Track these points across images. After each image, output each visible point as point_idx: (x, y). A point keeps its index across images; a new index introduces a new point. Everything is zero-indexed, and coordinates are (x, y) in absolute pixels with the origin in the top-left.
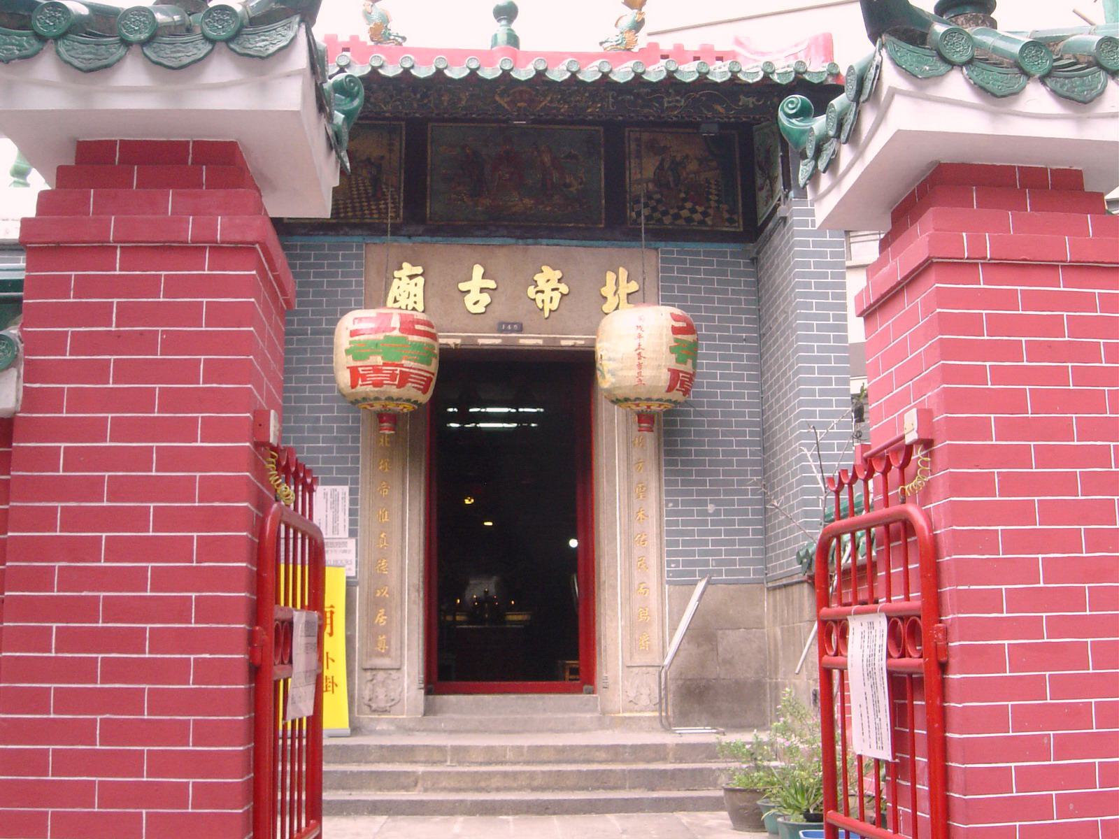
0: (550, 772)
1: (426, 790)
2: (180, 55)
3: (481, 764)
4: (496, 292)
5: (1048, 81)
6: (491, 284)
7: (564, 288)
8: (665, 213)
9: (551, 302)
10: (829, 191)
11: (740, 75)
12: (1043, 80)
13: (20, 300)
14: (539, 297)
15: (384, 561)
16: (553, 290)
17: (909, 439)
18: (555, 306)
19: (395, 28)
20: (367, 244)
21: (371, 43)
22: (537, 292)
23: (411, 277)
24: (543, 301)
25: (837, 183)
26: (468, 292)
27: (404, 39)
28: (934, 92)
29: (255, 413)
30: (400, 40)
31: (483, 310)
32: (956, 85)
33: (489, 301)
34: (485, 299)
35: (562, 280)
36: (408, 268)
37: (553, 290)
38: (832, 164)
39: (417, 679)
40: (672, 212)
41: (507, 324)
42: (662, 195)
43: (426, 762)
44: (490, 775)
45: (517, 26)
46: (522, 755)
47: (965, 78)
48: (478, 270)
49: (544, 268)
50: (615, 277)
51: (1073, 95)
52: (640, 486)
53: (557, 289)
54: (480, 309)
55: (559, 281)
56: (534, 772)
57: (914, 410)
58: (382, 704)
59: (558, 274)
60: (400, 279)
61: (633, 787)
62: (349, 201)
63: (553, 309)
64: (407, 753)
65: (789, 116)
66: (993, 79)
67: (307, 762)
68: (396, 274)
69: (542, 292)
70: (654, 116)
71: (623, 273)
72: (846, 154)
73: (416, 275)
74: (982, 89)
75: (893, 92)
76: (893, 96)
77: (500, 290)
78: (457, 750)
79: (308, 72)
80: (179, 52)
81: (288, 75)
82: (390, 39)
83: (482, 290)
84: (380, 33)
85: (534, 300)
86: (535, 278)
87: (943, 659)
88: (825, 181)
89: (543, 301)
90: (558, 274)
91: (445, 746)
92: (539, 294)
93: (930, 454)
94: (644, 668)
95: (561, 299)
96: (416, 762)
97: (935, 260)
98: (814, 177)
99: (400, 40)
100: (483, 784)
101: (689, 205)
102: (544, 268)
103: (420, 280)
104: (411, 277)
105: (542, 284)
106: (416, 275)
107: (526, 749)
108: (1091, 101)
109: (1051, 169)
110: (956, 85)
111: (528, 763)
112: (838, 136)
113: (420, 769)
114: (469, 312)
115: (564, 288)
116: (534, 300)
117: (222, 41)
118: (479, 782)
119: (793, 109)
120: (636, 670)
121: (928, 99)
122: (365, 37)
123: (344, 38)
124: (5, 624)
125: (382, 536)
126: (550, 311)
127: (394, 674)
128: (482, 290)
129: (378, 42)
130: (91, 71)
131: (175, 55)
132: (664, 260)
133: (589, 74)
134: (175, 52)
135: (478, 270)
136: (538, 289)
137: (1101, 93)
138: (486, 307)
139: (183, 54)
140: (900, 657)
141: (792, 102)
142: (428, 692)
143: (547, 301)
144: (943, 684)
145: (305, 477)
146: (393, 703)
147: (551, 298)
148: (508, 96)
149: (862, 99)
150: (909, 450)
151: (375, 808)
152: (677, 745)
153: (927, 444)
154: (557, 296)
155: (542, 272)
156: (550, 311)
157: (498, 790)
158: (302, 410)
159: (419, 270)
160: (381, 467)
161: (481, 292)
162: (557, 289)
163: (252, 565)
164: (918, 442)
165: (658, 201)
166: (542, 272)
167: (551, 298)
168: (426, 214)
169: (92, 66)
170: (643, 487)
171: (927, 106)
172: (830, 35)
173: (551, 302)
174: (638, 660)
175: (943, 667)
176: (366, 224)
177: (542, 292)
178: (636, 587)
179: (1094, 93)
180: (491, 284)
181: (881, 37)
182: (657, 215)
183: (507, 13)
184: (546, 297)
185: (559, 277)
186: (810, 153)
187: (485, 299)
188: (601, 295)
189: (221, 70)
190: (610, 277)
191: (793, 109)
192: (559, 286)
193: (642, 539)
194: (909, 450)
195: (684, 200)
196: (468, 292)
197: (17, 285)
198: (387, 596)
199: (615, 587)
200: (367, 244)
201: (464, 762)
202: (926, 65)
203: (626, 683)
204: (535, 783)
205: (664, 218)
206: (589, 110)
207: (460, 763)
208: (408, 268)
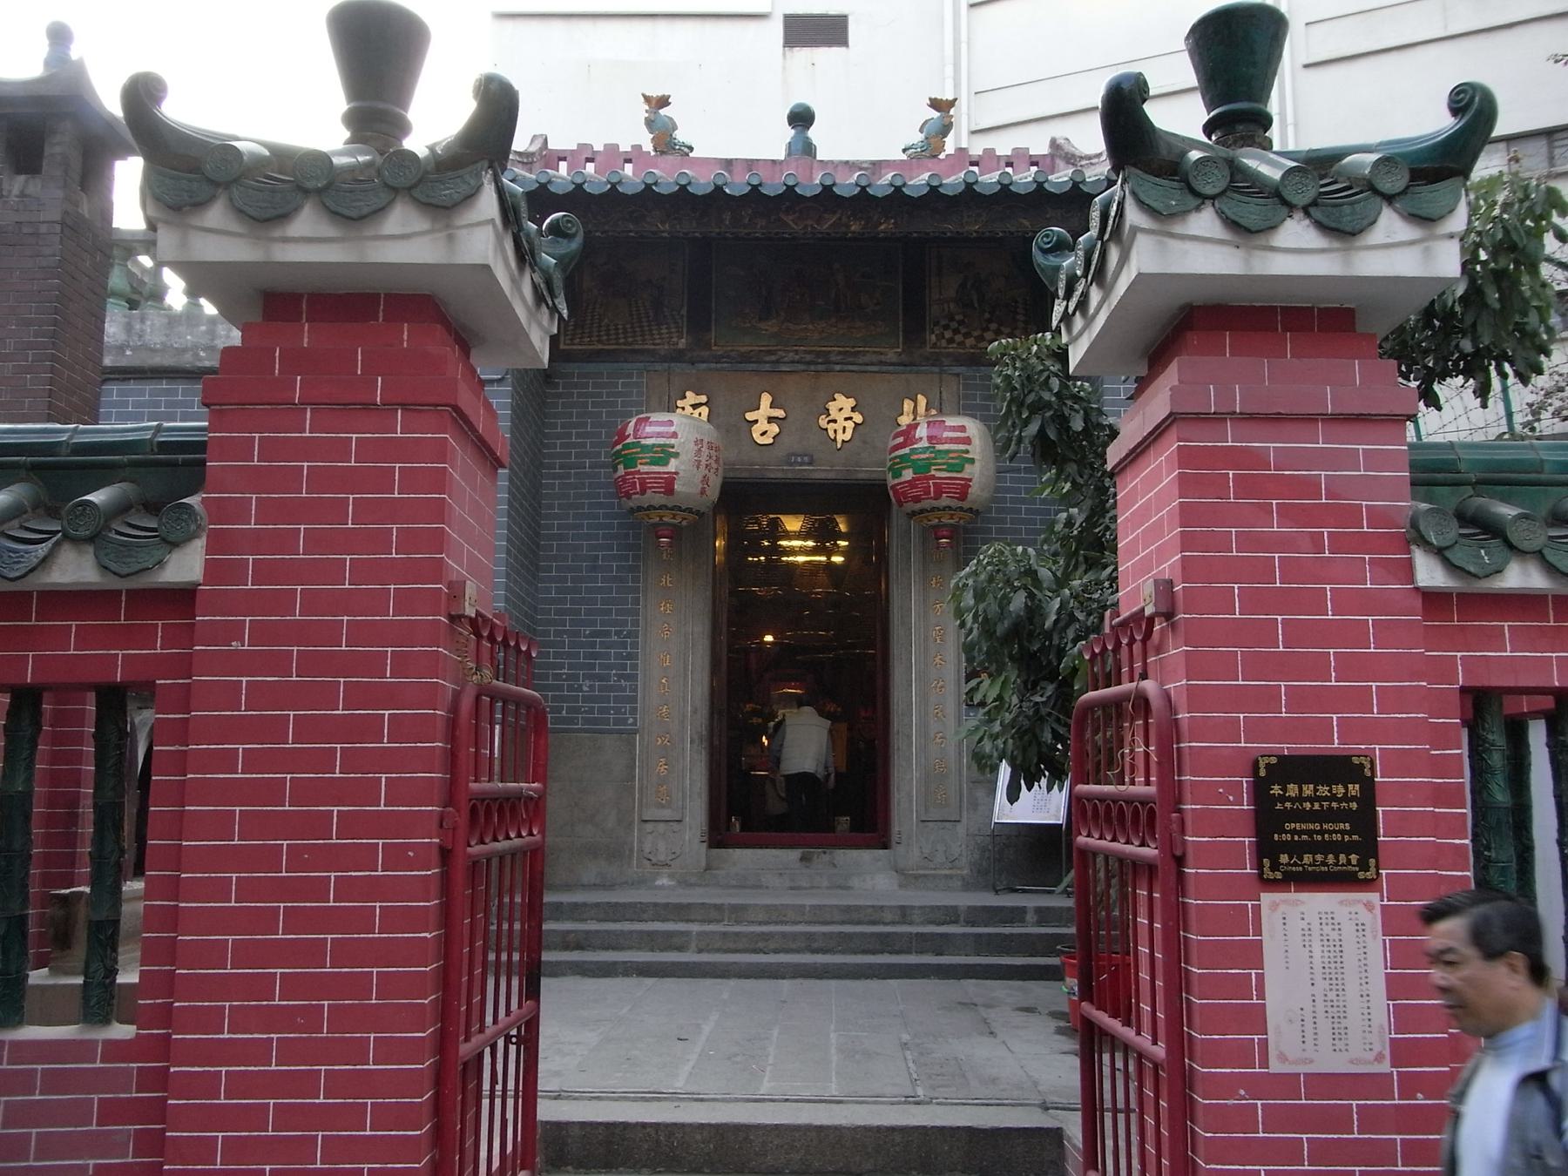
0: (832, 933)
1: (700, 951)
2: (358, 204)
3: (760, 923)
5: (1312, 210)
6: (780, 413)
7: (858, 418)
8: (967, 335)
9: (844, 432)
10: (1081, 333)
11: (1046, 185)
12: (1306, 210)
13: (203, 463)
14: (831, 427)
16: (846, 419)
17: (1149, 611)
18: (847, 436)
19: (681, 136)
20: (648, 371)
21: (653, 153)
22: (829, 422)
23: (695, 406)
24: (835, 431)
25: (1089, 321)
26: (756, 421)
27: (691, 149)
28: (1178, 229)
29: (450, 585)
30: (686, 150)
31: (771, 441)
32: (1204, 222)
33: (777, 430)
34: (775, 429)
36: (691, 397)
37: (846, 419)
38: (1083, 305)
40: (975, 334)
41: (796, 455)
42: (965, 316)
43: (703, 921)
44: (770, 936)
45: (813, 133)
46: (804, 914)
47: (1217, 212)
48: (766, 400)
49: (836, 396)
50: (912, 404)
51: (1341, 227)
53: (850, 418)
54: (768, 440)
55: (853, 409)
56: (815, 933)
57: (1152, 580)
58: (662, 858)
59: (852, 402)
60: (683, 408)
61: (921, 952)
62: (628, 326)
64: (681, 911)
65: (1045, 252)
66: (1250, 212)
68: (680, 403)
70: (951, 232)
71: (922, 400)
72: (1095, 295)
73: (701, 405)
74: (1232, 224)
75: (1135, 230)
76: (1135, 235)
77: (789, 420)
78: (736, 909)
79: (498, 221)
80: (360, 200)
81: (479, 224)
82: (674, 149)
83: (771, 420)
84: (666, 141)
85: (826, 429)
87: (1178, 853)
88: (1078, 322)
89: (835, 431)
90: (852, 402)
91: (723, 905)
93: (1173, 626)
96: (692, 921)
97: (1178, 416)
98: (1067, 318)
99: (686, 150)
100: (761, 945)
101: (993, 326)
102: (836, 396)
103: (705, 410)
104: (695, 406)
105: (834, 414)
106: (701, 405)
107: (808, 909)
108: (1361, 231)
109: (1318, 308)
110: (1204, 222)
111: (809, 923)
112: (1086, 277)
113: (695, 928)
115: (858, 418)
116: (826, 429)
117: (404, 188)
118: (757, 943)
119: (1049, 243)
120: (930, 824)
121: (1172, 236)
122: (648, 147)
123: (625, 147)
124: (187, 808)
126: (843, 441)
127: (675, 826)
128: (771, 420)
129: (663, 153)
130: (267, 220)
131: (354, 204)
132: (966, 387)
133: (883, 183)
134: (354, 201)
135: (766, 400)
136: (830, 418)
137: (1374, 222)
139: (362, 203)
140: (1140, 846)
141: (1047, 236)
142: (711, 846)
143: (840, 431)
144: (1181, 877)
145: (517, 644)
146: (674, 856)
147: (844, 428)
148: (794, 213)
149: (1106, 237)
150: (1151, 621)
151: (645, 971)
152: (969, 907)
153: (1169, 616)
154: (850, 425)
155: (835, 400)
157: (776, 951)
159: (703, 399)
161: (769, 422)
162: (850, 418)
163: (447, 744)
164: (1157, 614)
165: (961, 323)
166: (835, 400)
167: (844, 428)
169: (268, 216)
170: (939, 630)
171: (1174, 244)
173: (844, 432)
174: (935, 814)
175: (1180, 861)
176: (648, 351)
177: (835, 421)
178: (932, 736)
179: (1365, 222)
180: (780, 413)
181: (1124, 169)
182: (959, 338)
183: (801, 118)
186: (1061, 293)
187: (775, 429)
189: (401, 218)
190: (908, 405)
191: (1049, 243)
192: (853, 415)
194: (1151, 621)
195: (990, 321)
196: (756, 421)
197: (201, 447)
200: (648, 371)
201: (741, 922)
202: (1172, 199)
204: (815, 945)
205: (985, 334)
206: (882, 227)
207: (738, 922)
208: (691, 397)
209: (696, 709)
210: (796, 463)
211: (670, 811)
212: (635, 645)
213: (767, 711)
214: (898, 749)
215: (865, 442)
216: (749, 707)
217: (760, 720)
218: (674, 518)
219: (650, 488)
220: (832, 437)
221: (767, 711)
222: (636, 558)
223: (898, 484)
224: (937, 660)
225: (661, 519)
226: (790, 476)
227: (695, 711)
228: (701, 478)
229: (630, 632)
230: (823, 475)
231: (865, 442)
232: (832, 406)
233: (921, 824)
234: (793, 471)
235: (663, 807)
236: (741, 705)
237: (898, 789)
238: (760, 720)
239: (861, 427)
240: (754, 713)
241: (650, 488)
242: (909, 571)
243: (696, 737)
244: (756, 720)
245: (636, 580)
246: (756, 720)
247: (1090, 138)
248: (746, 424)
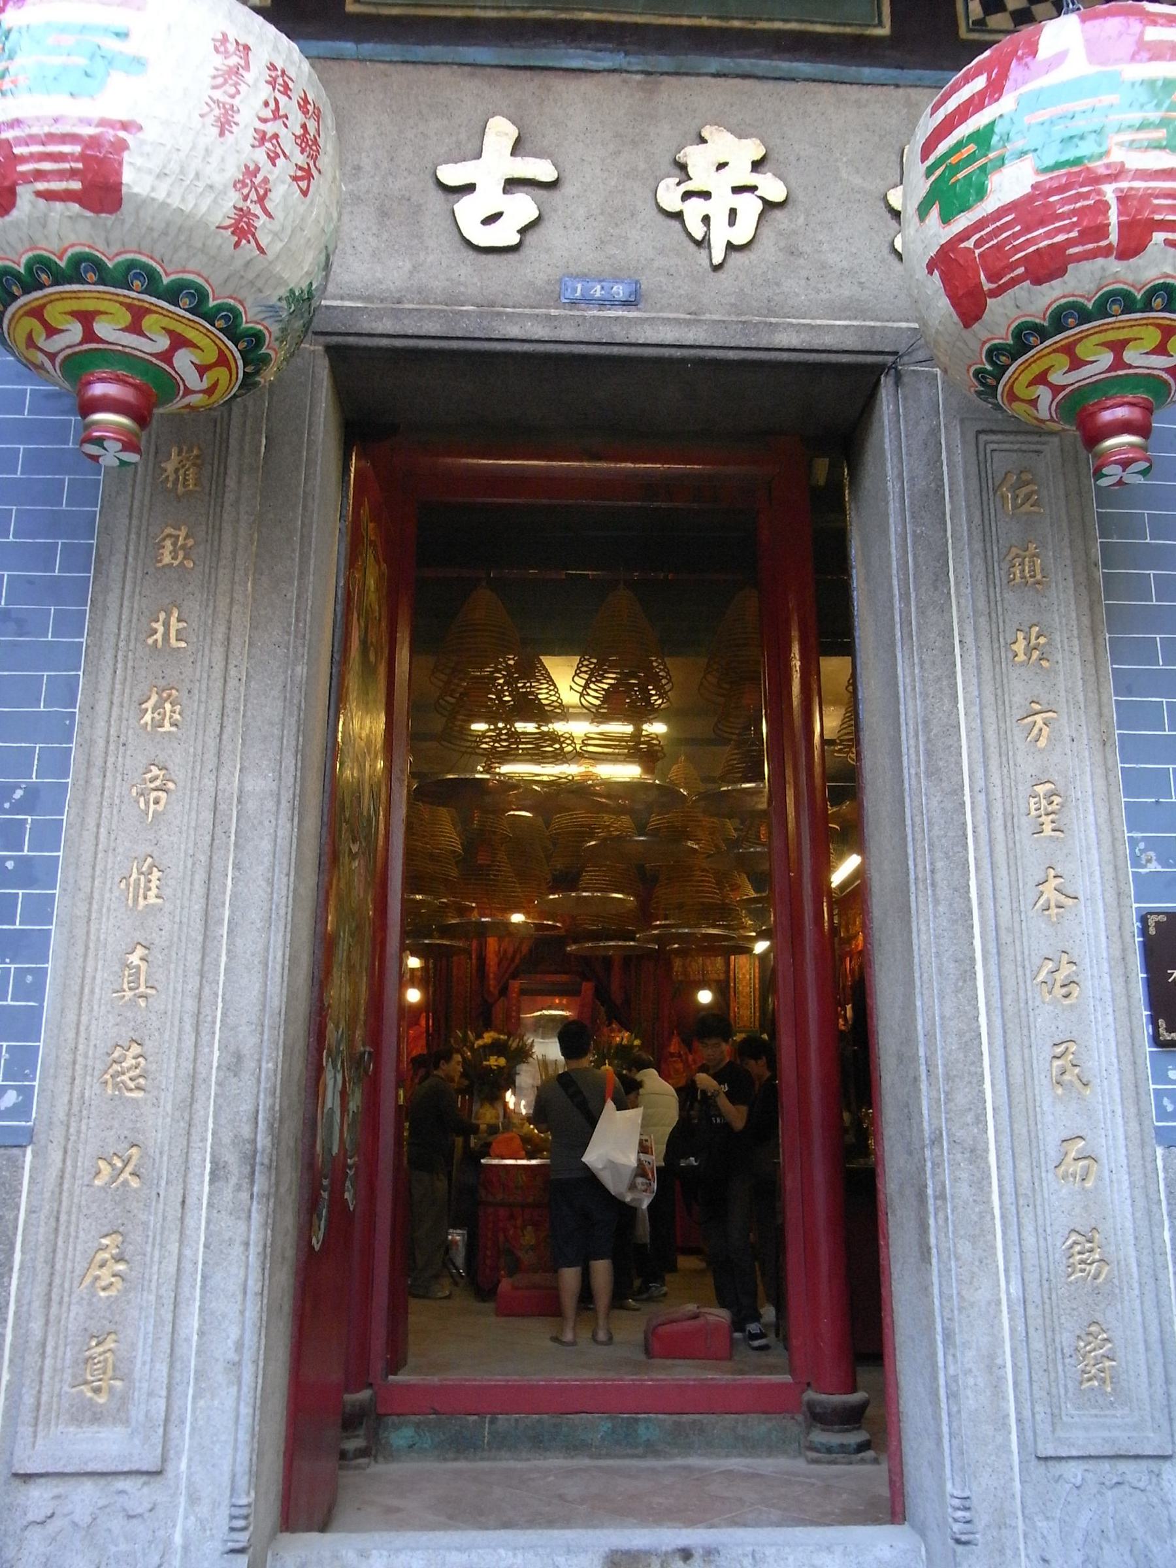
4: (556, 196)
14: (694, 210)
15: (135, 1049)
16: (737, 190)
18: (742, 233)
22: (687, 195)
24: (706, 219)
26: (470, 188)
31: (514, 239)
34: (522, 208)
35: (769, 165)
37: (737, 190)
39: (224, 1512)
52: (1041, 790)
53: (752, 189)
54: (504, 234)
63: (739, 241)
67: (812, 22)
69: (706, 195)
77: (568, 189)
83: (512, 184)
85: (678, 216)
86: (681, 157)
89: (706, 219)
90: (754, 149)
92: (694, 201)
94: (1106, 1466)
95: (761, 215)
114: (468, 243)
115: (773, 188)
116: (678, 216)
120: (1074, 1471)
125: (134, 959)
126: (730, 247)
127: (138, 1494)
128: (512, 184)
138: (523, 231)
147: (733, 212)
154: (749, 207)
155: (703, 141)
156: (730, 247)
158: (35, 461)
160: (148, 718)
162: (752, 189)
166: (703, 141)
167: (733, 212)
168: (909, 329)
170: (1050, 795)
172: (752, 171)
177: (706, 195)
178: (1053, 1154)
180: (543, 170)
184: (717, 209)
185: (758, 157)
187: (522, 208)
188: (438, 180)
193: (1060, 977)
196: (470, 188)
198: (134, 1183)
199: (977, 1154)
203: (1042, 1524)
209: (239, 1057)
210: (588, 301)
211: (120, 1431)
212: (49, 835)
213: (514, 1044)
214: (941, 1196)
215: (792, 252)
216: (488, 1037)
217: (502, 1061)
218: (135, 328)
219: (28, 178)
220: (698, 234)
221: (514, 1044)
222: (77, 558)
223: (964, 235)
224: (1049, 890)
225: (89, 335)
226: (568, 333)
227: (234, 1064)
228: (234, 172)
229: (33, 793)
230: (668, 335)
231: (792, 252)
232: (697, 158)
233: (1039, 1470)
234: (581, 322)
235: (97, 1417)
236: (471, 1035)
237: (948, 1336)
238: (502, 1061)
239: (778, 214)
240: (498, 1048)
241: (28, 178)
242: (945, 609)
243: (231, 1158)
244: (495, 1062)
245: (71, 624)
246: (495, 1062)
247: (370, 1381)
248: (437, 196)
